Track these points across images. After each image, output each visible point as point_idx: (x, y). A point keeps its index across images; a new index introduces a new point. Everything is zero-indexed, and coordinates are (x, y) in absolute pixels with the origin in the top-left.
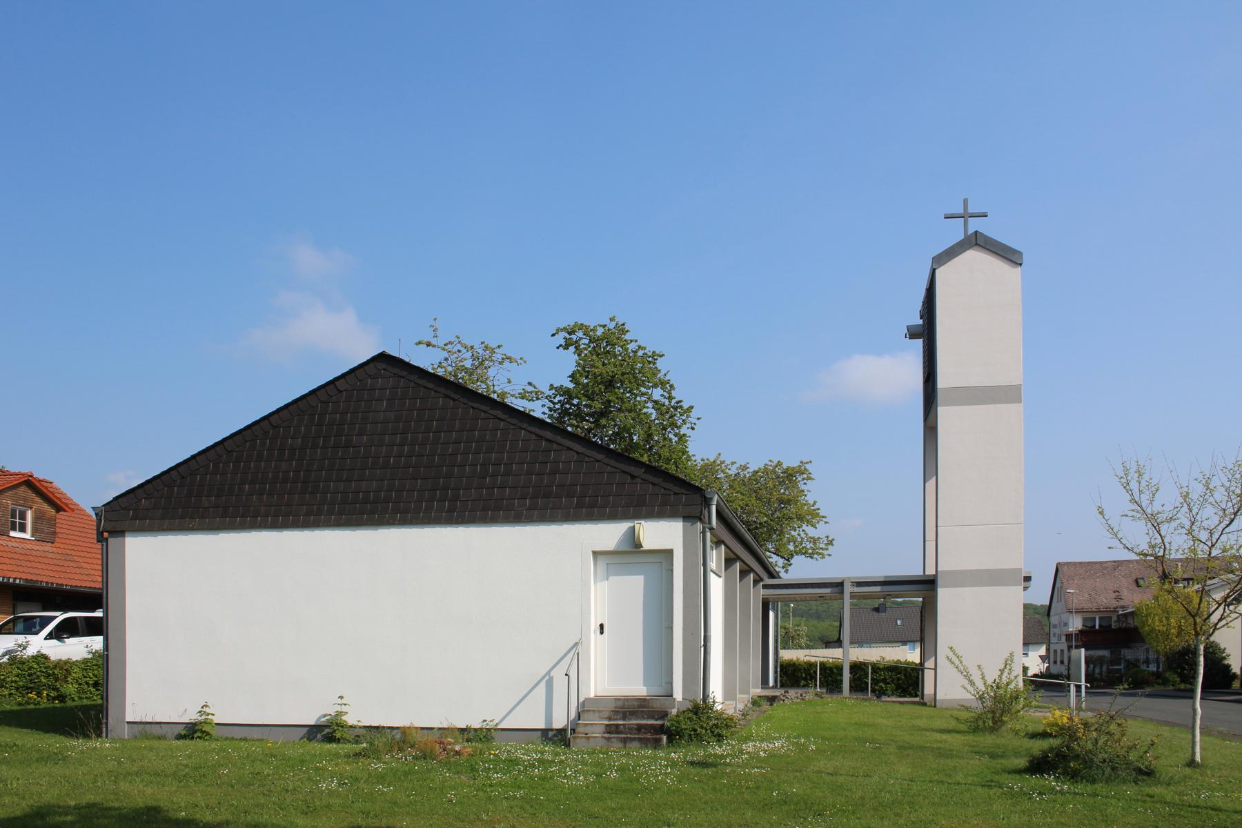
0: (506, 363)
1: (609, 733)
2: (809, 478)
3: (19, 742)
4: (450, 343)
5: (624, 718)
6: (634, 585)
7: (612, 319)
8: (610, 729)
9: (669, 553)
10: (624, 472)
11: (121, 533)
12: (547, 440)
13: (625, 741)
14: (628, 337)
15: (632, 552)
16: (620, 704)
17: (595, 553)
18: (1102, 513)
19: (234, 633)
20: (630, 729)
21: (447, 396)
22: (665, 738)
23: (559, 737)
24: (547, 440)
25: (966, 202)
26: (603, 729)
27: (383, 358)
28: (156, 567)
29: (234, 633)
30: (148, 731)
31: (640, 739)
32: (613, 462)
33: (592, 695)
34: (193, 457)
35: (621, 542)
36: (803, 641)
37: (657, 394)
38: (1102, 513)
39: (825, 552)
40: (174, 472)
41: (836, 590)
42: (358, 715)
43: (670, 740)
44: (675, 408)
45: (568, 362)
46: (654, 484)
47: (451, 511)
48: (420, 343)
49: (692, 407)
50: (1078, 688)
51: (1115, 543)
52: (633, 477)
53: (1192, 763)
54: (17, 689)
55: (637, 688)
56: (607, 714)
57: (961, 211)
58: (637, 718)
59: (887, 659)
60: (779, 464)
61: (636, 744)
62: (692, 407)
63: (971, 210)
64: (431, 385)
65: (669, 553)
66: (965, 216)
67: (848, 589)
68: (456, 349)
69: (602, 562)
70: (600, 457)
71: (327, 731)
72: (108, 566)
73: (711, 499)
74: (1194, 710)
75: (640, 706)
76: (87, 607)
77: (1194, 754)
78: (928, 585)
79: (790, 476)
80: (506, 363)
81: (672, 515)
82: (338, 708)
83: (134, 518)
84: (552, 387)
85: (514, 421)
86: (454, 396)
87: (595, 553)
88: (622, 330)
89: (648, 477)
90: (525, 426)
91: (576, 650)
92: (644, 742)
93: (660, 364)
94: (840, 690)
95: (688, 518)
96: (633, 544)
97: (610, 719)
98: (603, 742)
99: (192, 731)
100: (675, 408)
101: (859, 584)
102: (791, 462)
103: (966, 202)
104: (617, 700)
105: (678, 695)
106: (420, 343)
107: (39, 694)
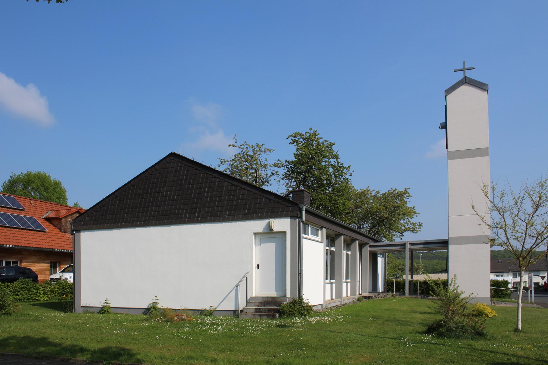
0: (268, 152)
1: (256, 312)
2: (409, 196)
3: (31, 313)
4: (243, 145)
5: (264, 306)
6: (271, 247)
7: (311, 129)
8: (257, 310)
9: (285, 233)
10: (266, 198)
11: (78, 231)
12: (235, 185)
13: (261, 316)
14: (319, 136)
15: (269, 234)
16: (264, 299)
17: (255, 234)
18: (473, 208)
19: (126, 271)
20: (264, 310)
21: (196, 169)
22: (277, 315)
23: (236, 313)
24: (235, 185)
25: (464, 63)
26: (254, 310)
27: (173, 155)
28: (94, 245)
29: (126, 271)
30: (88, 309)
31: (267, 315)
32: (262, 194)
33: (254, 295)
34: (104, 199)
35: (265, 229)
36: (421, 271)
37: (333, 161)
38: (473, 208)
39: (418, 230)
40: (97, 206)
41: (402, 247)
42: (163, 304)
43: (280, 316)
44: (341, 167)
45: (293, 149)
46: (278, 203)
47: (198, 217)
48: (229, 146)
49: (350, 166)
50: (531, 291)
51: (482, 222)
52: (270, 200)
53: (516, 330)
54: (58, 294)
55: (273, 293)
56: (257, 304)
57: (462, 67)
58: (270, 306)
59: (441, 279)
60: (396, 189)
61: (265, 317)
62: (350, 166)
63: (467, 67)
64: (190, 165)
65: (285, 233)
66: (464, 70)
67: (408, 247)
68: (245, 147)
69: (258, 237)
70: (256, 192)
71: (150, 311)
72: (75, 243)
73: (302, 208)
74: (518, 304)
75: (272, 301)
76: (67, 258)
77: (517, 325)
78: (445, 244)
79: (401, 195)
80: (268, 152)
81: (285, 216)
82: (154, 301)
83: (83, 225)
84: (286, 161)
85: (222, 178)
86: (200, 169)
87: (255, 234)
88: (315, 134)
89: (275, 199)
90: (227, 180)
91: (246, 278)
92: (269, 316)
93: (334, 148)
94: (404, 293)
95: (293, 217)
96: (269, 230)
97: (258, 306)
98: (252, 316)
99: (103, 310)
100: (341, 167)
101: (413, 244)
102: (401, 189)
103: (464, 63)
104: (263, 298)
105: (289, 295)
106: (229, 146)
107: (67, 296)
